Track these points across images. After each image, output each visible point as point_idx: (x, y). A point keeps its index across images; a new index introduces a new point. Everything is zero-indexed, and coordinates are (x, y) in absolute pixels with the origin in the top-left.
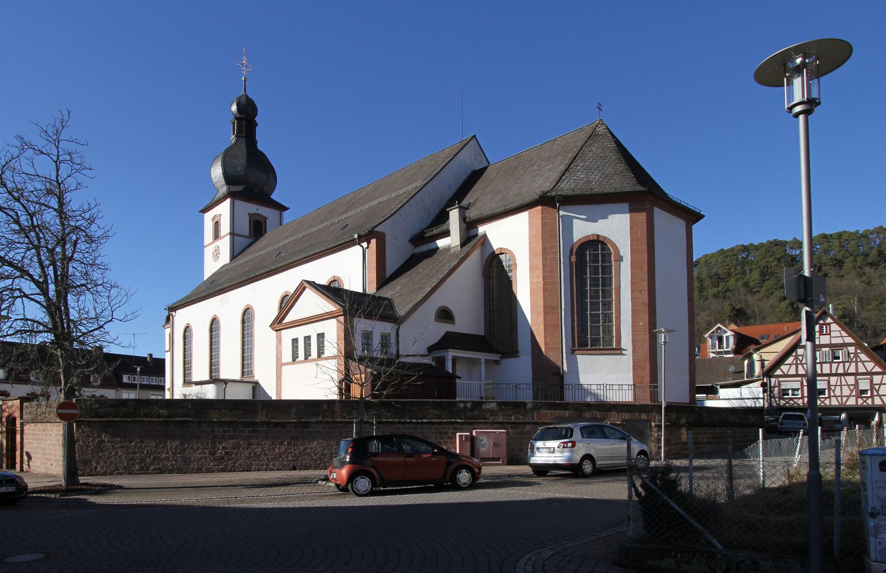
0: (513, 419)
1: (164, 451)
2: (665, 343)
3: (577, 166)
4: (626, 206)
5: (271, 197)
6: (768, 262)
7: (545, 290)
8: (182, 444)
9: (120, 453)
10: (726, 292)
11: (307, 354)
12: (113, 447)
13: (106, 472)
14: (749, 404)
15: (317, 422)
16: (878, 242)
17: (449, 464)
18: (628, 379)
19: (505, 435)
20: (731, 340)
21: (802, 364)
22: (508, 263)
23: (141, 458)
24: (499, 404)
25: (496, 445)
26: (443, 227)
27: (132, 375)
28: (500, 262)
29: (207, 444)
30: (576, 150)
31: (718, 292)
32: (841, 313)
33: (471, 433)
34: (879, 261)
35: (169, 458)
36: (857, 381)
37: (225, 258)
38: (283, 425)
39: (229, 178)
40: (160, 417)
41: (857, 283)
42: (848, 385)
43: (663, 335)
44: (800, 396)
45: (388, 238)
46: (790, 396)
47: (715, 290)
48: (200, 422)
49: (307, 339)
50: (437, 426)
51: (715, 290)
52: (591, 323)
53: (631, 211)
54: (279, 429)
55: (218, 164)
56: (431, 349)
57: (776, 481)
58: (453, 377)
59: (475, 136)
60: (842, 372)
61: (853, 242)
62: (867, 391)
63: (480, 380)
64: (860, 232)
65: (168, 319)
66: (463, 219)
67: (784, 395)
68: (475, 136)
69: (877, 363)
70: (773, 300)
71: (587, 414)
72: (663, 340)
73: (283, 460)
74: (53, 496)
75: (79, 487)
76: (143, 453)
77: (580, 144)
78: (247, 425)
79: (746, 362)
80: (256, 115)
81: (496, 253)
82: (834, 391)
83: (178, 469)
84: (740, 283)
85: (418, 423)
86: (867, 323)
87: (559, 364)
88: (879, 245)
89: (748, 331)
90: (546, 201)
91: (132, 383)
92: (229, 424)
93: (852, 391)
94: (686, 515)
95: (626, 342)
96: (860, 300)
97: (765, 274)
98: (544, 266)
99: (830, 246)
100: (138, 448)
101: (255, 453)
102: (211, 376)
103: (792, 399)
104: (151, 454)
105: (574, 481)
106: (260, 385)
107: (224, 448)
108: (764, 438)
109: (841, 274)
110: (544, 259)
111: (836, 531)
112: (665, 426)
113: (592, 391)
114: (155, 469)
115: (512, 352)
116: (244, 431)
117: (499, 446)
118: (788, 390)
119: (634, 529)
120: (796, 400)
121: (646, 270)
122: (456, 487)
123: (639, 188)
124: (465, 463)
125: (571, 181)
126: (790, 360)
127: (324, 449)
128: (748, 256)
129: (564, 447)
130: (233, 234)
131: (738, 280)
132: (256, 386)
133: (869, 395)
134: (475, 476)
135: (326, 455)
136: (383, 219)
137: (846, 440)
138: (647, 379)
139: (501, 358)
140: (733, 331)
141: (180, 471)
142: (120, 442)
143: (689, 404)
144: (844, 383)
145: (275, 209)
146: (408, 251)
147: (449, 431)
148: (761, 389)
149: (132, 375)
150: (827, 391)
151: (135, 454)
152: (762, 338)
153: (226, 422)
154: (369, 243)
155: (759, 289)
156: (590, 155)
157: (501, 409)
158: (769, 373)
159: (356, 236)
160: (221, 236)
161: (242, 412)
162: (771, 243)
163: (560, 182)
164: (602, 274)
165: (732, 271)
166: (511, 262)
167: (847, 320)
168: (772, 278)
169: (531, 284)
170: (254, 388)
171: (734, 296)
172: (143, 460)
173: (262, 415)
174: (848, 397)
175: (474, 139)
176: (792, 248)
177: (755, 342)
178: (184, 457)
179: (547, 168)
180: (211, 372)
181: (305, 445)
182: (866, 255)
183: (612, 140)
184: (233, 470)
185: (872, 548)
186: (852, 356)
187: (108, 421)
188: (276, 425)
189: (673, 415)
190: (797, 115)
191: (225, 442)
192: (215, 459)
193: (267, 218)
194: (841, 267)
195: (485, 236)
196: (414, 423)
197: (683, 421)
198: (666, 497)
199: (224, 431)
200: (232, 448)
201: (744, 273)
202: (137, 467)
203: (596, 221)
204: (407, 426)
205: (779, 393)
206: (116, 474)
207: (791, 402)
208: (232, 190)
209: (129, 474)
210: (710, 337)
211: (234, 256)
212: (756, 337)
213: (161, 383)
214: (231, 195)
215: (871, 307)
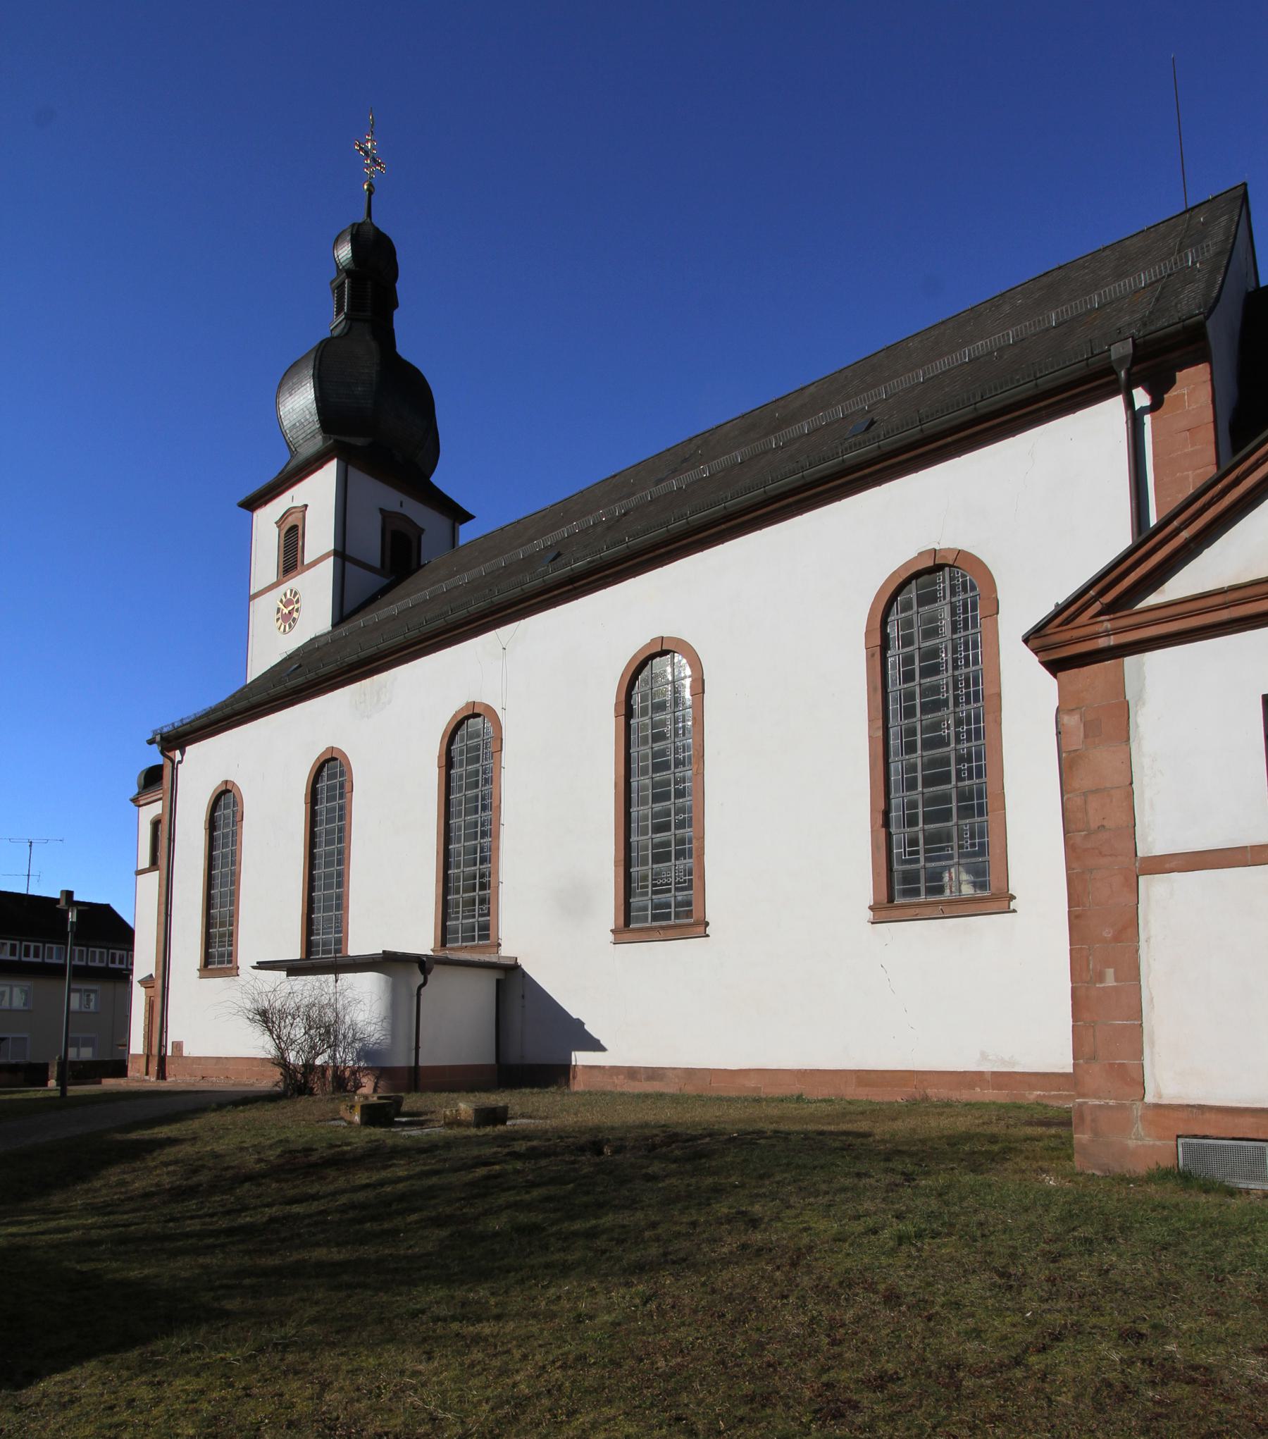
27: (21, 942)
55: (300, 382)
65: (153, 778)
91: (20, 963)
102: (309, 946)
106: (524, 974)
130: (341, 555)
145: (442, 513)
149: (21, 942)
180: (309, 926)
193: (422, 530)
211: (342, 615)
213: (51, 958)
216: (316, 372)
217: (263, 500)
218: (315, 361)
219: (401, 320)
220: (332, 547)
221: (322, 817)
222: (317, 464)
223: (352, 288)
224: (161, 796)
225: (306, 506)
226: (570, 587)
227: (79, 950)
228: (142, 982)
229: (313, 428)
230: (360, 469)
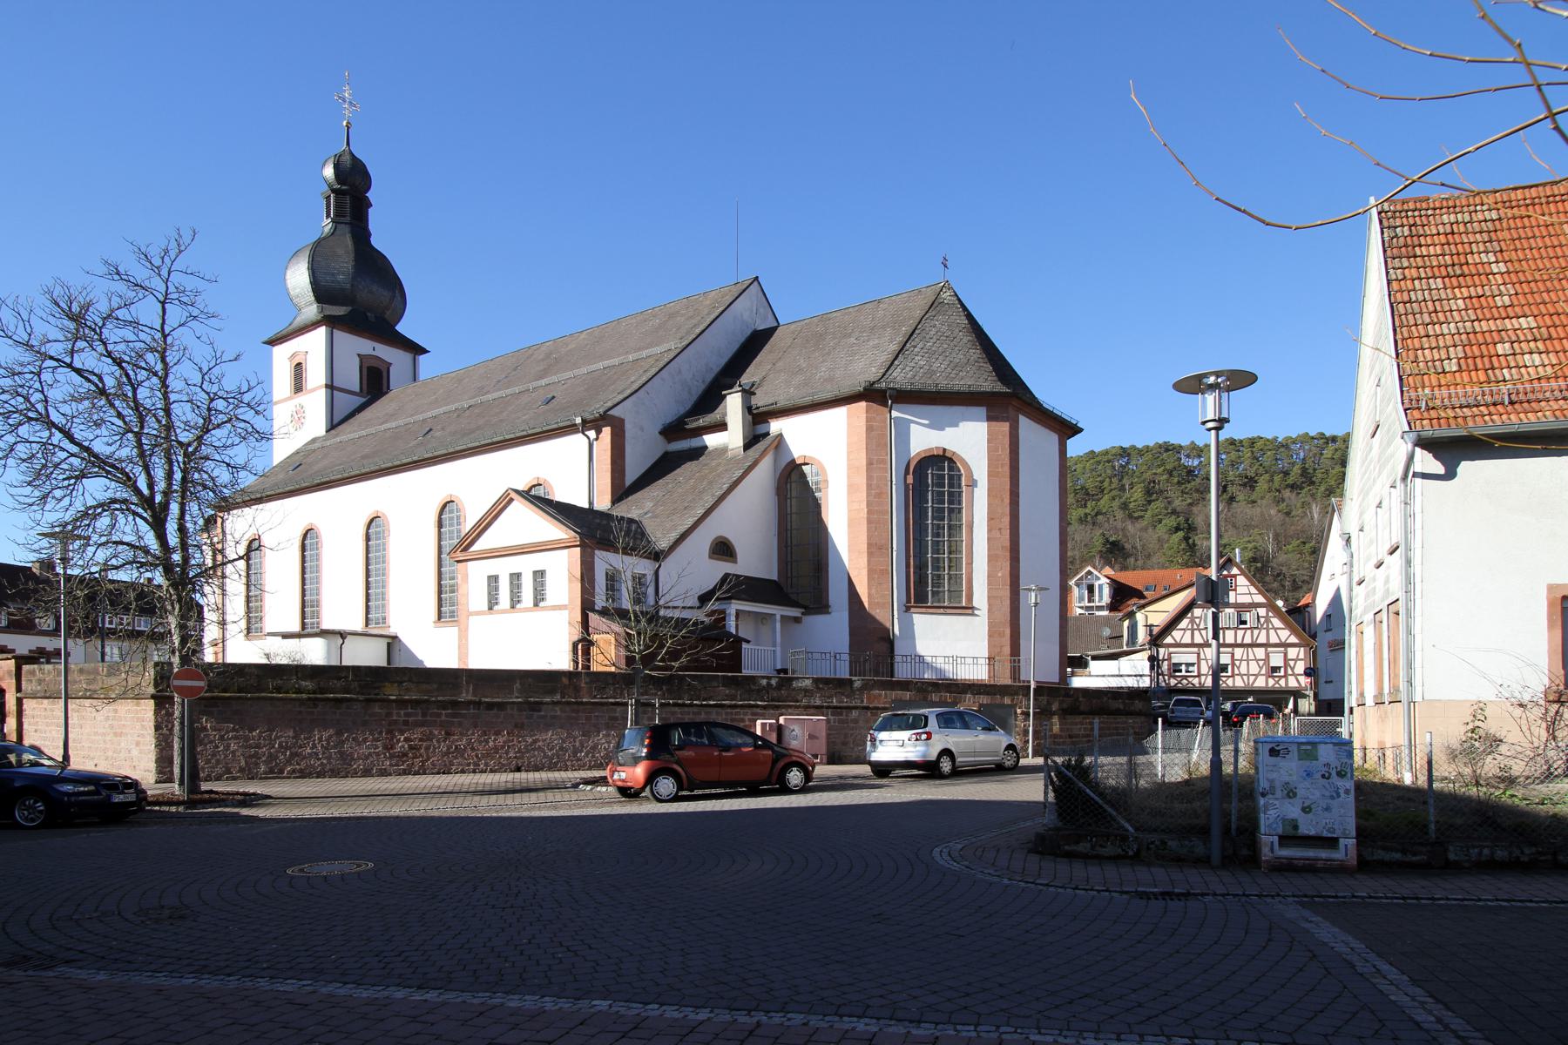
0: (835, 702)
1: (308, 743)
2: (1036, 604)
3: (915, 347)
4: (982, 411)
5: (398, 328)
6: (1155, 474)
7: (869, 522)
8: (339, 733)
9: (233, 747)
10: (1096, 515)
11: (515, 601)
12: (222, 738)
13: (209, 776)
14: (1131, 683)
15: (554, 703)
16: (1302, 455)
17: (775, 762)
18: (982, 650)
19: (824, 724)
20: (1106, 591)
21: (1199, 630)
22: (815, 479)
23: (270, 755)
24: (816, 681)
25: (811, 737)
26: (713, 417)
28: (803, 475)
29: (381, 733)
30: (913, 323)
31: (1086, 515)
32: (1251, 554)
33: (778, 721)
34: (1303, 483)
35: (316, 754)
36: (1267, 655)
37: (316, 424)
38: (501, 706)
39: (322, 293)
40: (302, 693)
41: (1273, 512)
42: (1257, 660)
43: (1033, 594)
44: (1196, 674)
45: (628, 426)
46: (1183, 673)
47: (1081, 512)
48: (368, 701)
49: (516, 578)
50: (729, 710)
51: (1081, 512)
52: (933, 570)
53: (989, 419)
54: (495, 711)
56: (704, 599)
57: (1177, 775)
58: (738, 641)
59: (756, 279)
60: (1249, 642)
61: (1269, 453)
62: (1279, 668)
63: (775, 645)
64: (1280, 440)
66: (748, 409)
67: (1175, 671)
68: (756, 279)
69: (1294, 631)
70: (1161, 530)
71: (935, 697)
72: (1033, 601)
73: (500, 757)
74: (173, 809)
75: (199, 796)
76: (273, 747)
77: (918, 313)
78: (443, 705)
79: (1126, 623)
80: (369, 188)
81: (798, 462)
82: (1238, 668)
83: (332, 770)
84: (1116, 503)
85: (702, 705)
86: (1284, 569)
87: (888, 625)
88: (1304, 459)
89: (1129, 578)
90: (873, 394)
92: (417, 703)
93: (1261, 668)
94: (1100, 802)
95: (980, 598)
96: (1276, 536)
97: (1150, 493)
98: (869, 486)
99: (1239, 457)
100: (265, 739)
101: (456, 747)
102: (304, 625)
103: (1185, 677)
104: (287, 748)
105: (931, 782)
106: (400, 641)
107: (406, 740)
108: (1164, 729)
109: (1253, 498)
110: (869, 478)
111: (1233, 811)
112: (1034, 713)
113: (938, 666)
114: (294, 771)
115: (819, 605)
116: (439, 715)
117: (816, 738)
118: (1181, 664)
119: (1050, 819)
120: (1190, 679)
121: (1007, 501)
122: (785, 790)
123: (1000, 388)
124: (794, 759)
125: (908, 369)
126: (1184, 623)
127: (564, 742)
128: (1127, 463)
129: (917, 740)
130: (331, 387)
131: (1114, 499)
132: (393, 642)
133: (1282, 673)
134: (808, 777)
135: (567, 751)
136: (621, 397)
137: (1249, 733)
138: (1007, 650)
139: (803, 614)
140: (1109, 578)
141: (335, 774)
142: (234, 730)
143: (1059, 684)
144: (1251, 657)
145: (405, 350)
146: (659, 447)
147: (747, 718)
148: (1147, 664)
150: (1230, 667)
151: (259, 748)
152: (1147, 589)
153: (410, 701)
154: (599, 432)
155: (1142, 514)
156: (932, 333)
157: (818, 688)
158: (1156, 640)
159: (578, 420)
160: (309, 388)
161: (435, 686)
162: (1160, 446)
163: (892, 368)
164: (949, 504)
165: (1106, 484)
166: (820, 478)
167: (1259, 565)
168: (1161, 499)
169: (849, 511)
170: (389, 645)
171: (1108, 521)
172: (272, 758)
173: (467, 692)
174: (1256, 676)
175: (756, 283)
176: (1188, 456)
177: (1139, 594)
178: (342, 753)
179: (871, 343)
181: (535, 735)
182: (1286, 473)
183: (962, 314)
184: (422, 771)
185: (1262, 822)
186: (1262, 620)
187: (213, 698)
188: (490, 706)
189: (1044, 699)
190: (1209, 430)
191: (409, 730)
192: (392, 757)
194: (1253, 488)
195: (780, 437)
196: (696, 705)
197: (1055, 707)
198: (1081, 785)
199: (407, 715)
200: (421, 740)
201: (1122, 489)
202: (263, 768)
203: (942, 429)
204: (686, 709)
205: (1169, 669)
206: (227, 779)
207: (1185, 682)
208: (328, 313)
209: (249, 779)
210: (1077, 585)
211: (334, 424)
212: (1140, 588)
214: (330, 321)
215: (1290, 547)
219: (374, 216)
221: (308, 559)
223: (336, 200)
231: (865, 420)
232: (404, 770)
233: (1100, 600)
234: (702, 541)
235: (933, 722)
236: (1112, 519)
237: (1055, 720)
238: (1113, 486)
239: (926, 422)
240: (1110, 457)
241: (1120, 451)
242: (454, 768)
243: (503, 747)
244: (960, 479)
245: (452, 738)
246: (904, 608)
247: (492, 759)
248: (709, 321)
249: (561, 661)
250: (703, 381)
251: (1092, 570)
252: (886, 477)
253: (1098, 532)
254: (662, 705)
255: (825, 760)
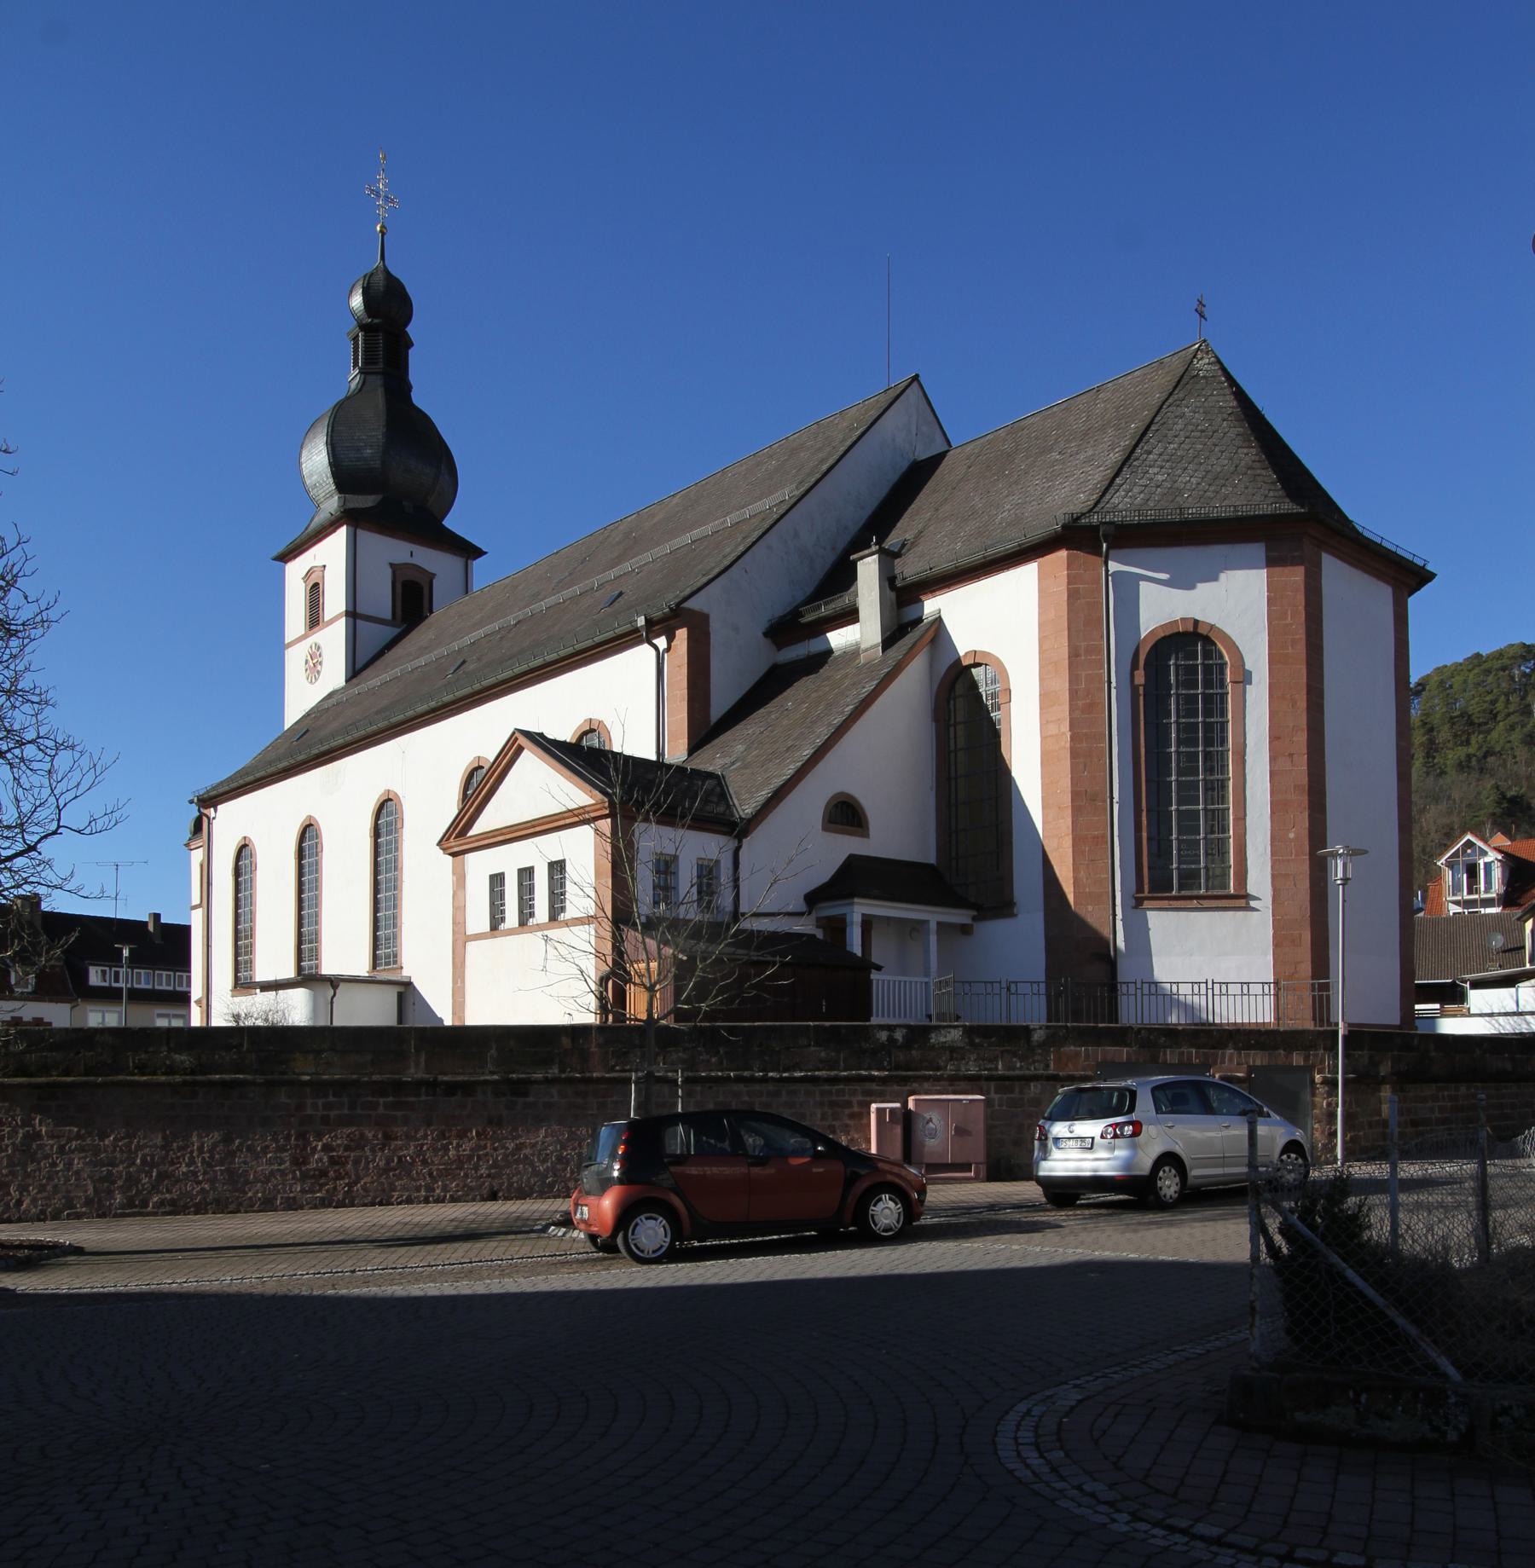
1: (184, 1156)
2: (1345, 880)
3: (1149, 453)
4: (1258, 550)
5: (443, 523)
7: (1074, 754)
9: (77, 1164)
10: (1485, 757)
12: (61, 1149)
13: (43, 1212)
15: (547, 1081)
17: (852, 1180)
18: (1262, 967)
19: (981, 1108)
20: (1497, 873)
22: (991, 688)
23: (129, 1175)
24: (970, 1031)
25: (961, 1132)
26: (841, 602)
27: (111, 967)
28: (974, 685)
29: (288, 1138)
30: (1147, 414)
31: (1469, 757)
33: (905, 1104)
35: (195, 1174)
37: (334, 675)
38: (467, 1088)
39: (344, 476)
40: (175, 1073)
45: (715, 626)
47: (1462, 752)
50: (826, 1087)
51: (1462, 752)
52: (1179, 833)
53: (1271, 563)
56: (813, 898)
58: (864, 966)
59: (916, 378)
66: (888, 579)
68: (917, 376)
71: (1170, 1056)
72: (1340, 875)
73: (466, 1176)
76: (134, 1163)
77: (1157, 398)
78: (381, 1089)
80: (408, 319)
81: (965, 663)
83: (217, 1201)
84: (1516, 736)
85: (782, 1080)
87: (1106, 932)
92: (341, 1086)
94: (1380, 1301)
95: (1259, 879)
98: (1073, 694)
101: (400, 1159)
102: (299, 969)
104: (153, 1165)
107: (327, 1148)
110: (1073, 679)
114: (162, 1203)
115: (999, 904)
121: (1302, 704)
122: (868, 1237)
123: (1288, 507)
124: (889, 1177)
125: (1136, 490)
127: (564, 1148)
129: (1115, 1136)
130: (352, 614)
131: (1512, 728)
132: (406, 992)
134: (911, 1210)
135: (568, 1163)
136: (705, 579)
138: (1306, 968)
141: (223, 1207)
142: (79, 1137)
146: (764, 657)
147: (854, 1100)
154: (670, 640)
157: (972, 1043)
159: (641, 621)
163: (1111, 491)
165: (1500, 705)
170: (401, 996)
172: (132, 1180)
175: (915, 384)
178: (231, 1172)
181: (520, 1137)
183: (1227, 391)
184: (348, 1202)
187: (48, 1085)
188: (452, 1088)
189: (1363, 1056)
192: (305, 1176)
195: (938, 621)
197: (1385, 1069)
198: (1335, 1259)
199: (327, 1106)
200: (347, 1148)
203: (1191, 587)
204: (757, 1087)
206: (69, 1217)
208: (351, 505)
209: (99, 1216)
210: (1450, 865)
211: (355, 671)
213: (140, 983)
214: (349, 517)
216: (329, 439)
217: (292, 555)
218: (327, 435)
220: (344, 609)
222: (332, 528)
223: (365, 341)
224: (201, 844)
225: (324, 566)
226: (433, 715)
227: (167, 975)
228: (196, 1002)
229: (330, 489)
230: (370, 530)
231: (1065, 581)
232: (322, 1199)
233: (1488, 889)
234: (811, 800)
235: (1145, 1104)
236: (1510, 761)
237: (1386, 1092)
238: (1512, 708)
239: (1164, 576)
240: (1506, 661)
241: (1521, 651)
242: (396, 1194)
243: (470, 1158)
244: (1222, 672)
245: (393, 1144)
246: (1133, 902)
247: (454, 1179)
248: (842, 449)
249: (586, 1016)
250: (834, 548)
251: (1473, 839)
252: (1101, 675)
253: (1489, 783)
254: (686, 1080)
255: (983, 1174)
